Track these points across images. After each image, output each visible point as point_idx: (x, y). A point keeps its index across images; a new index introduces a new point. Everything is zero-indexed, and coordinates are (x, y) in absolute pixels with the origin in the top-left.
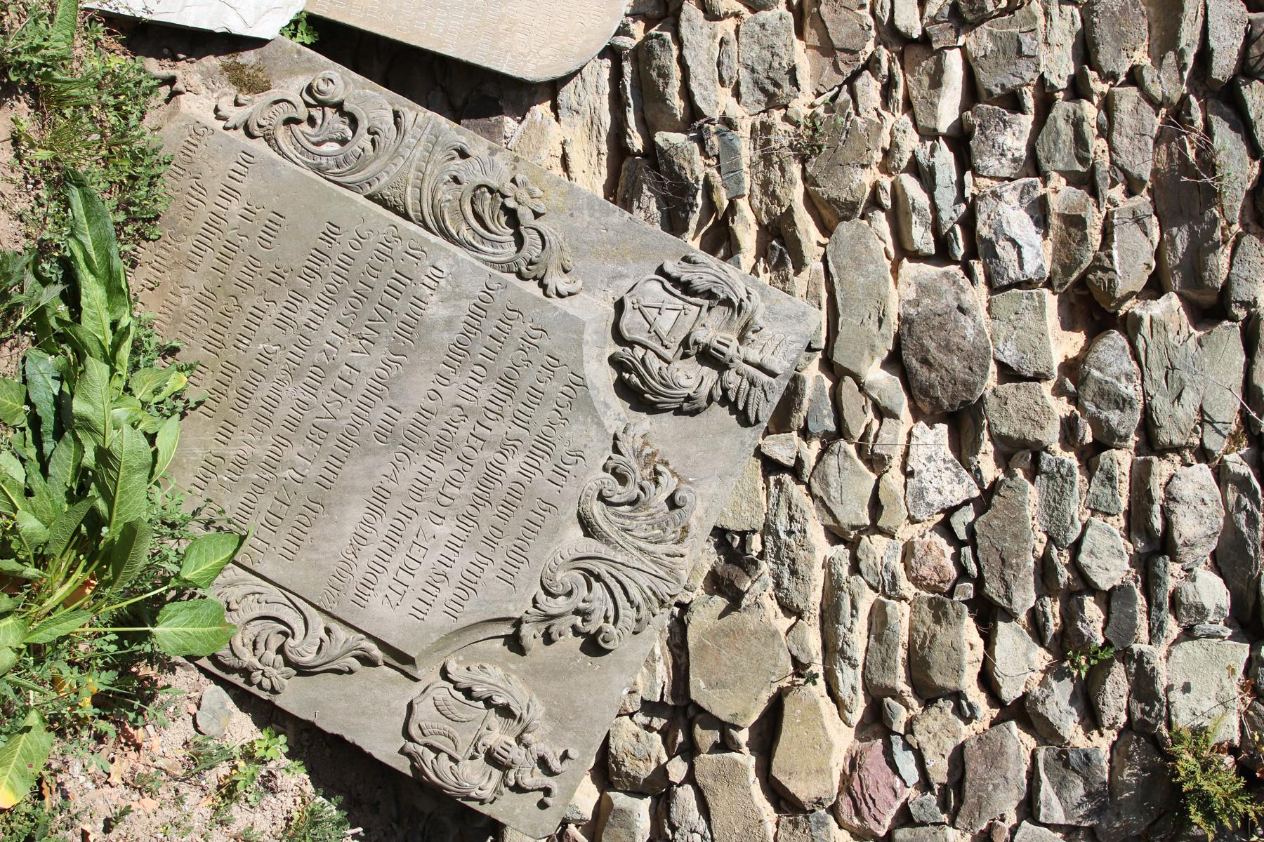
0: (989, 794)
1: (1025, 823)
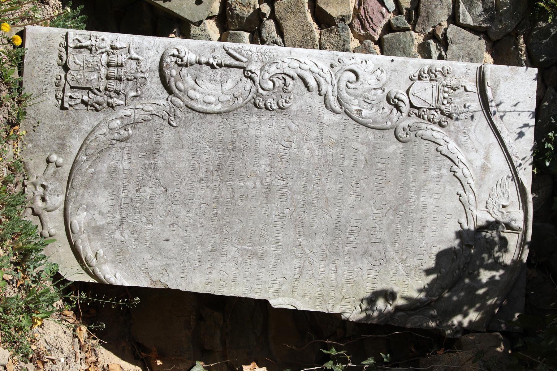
0: (432, 10)
1: (452, 26)
